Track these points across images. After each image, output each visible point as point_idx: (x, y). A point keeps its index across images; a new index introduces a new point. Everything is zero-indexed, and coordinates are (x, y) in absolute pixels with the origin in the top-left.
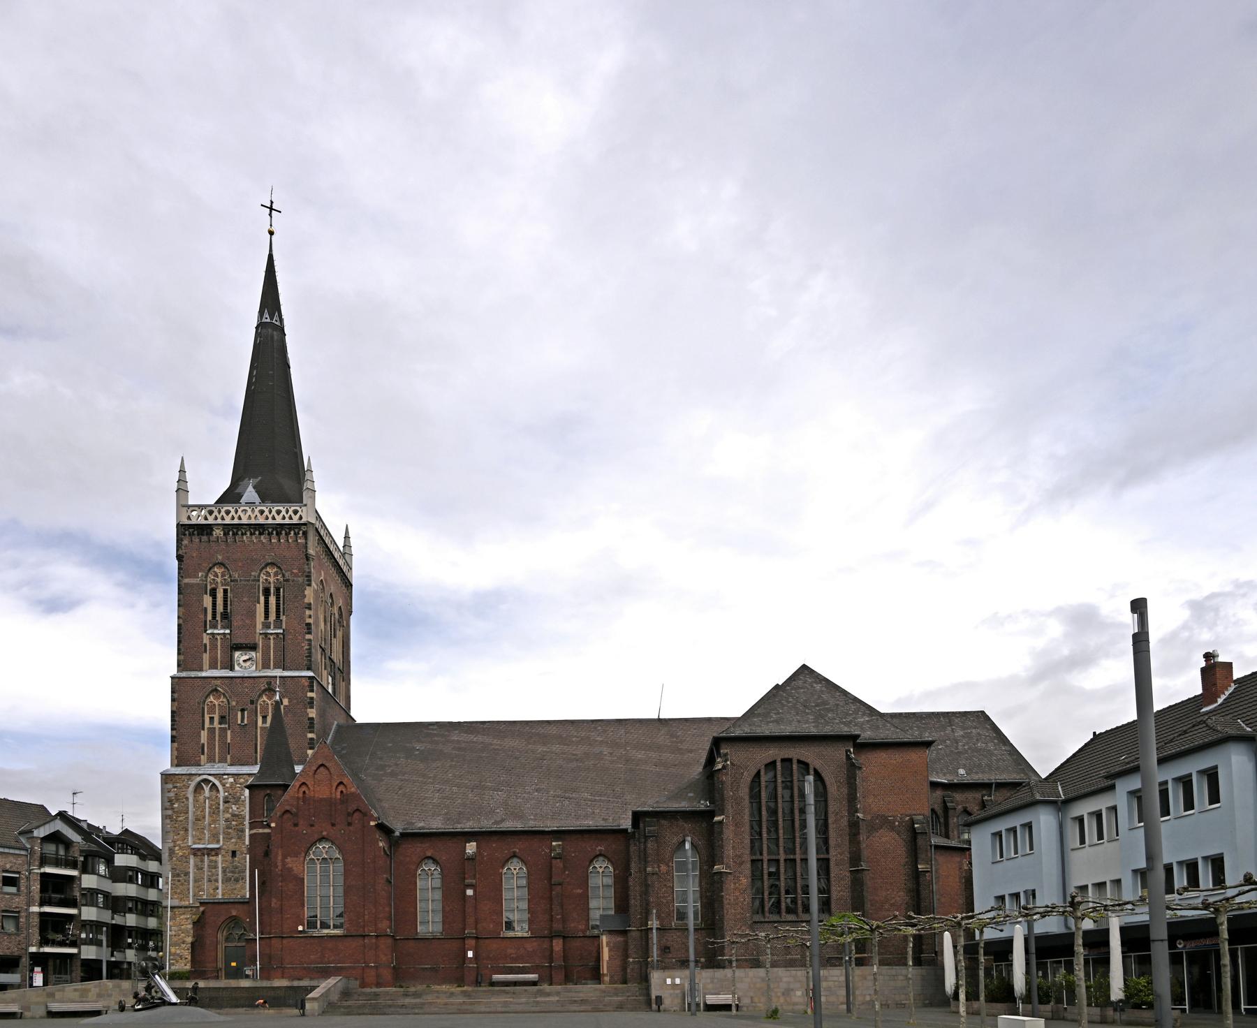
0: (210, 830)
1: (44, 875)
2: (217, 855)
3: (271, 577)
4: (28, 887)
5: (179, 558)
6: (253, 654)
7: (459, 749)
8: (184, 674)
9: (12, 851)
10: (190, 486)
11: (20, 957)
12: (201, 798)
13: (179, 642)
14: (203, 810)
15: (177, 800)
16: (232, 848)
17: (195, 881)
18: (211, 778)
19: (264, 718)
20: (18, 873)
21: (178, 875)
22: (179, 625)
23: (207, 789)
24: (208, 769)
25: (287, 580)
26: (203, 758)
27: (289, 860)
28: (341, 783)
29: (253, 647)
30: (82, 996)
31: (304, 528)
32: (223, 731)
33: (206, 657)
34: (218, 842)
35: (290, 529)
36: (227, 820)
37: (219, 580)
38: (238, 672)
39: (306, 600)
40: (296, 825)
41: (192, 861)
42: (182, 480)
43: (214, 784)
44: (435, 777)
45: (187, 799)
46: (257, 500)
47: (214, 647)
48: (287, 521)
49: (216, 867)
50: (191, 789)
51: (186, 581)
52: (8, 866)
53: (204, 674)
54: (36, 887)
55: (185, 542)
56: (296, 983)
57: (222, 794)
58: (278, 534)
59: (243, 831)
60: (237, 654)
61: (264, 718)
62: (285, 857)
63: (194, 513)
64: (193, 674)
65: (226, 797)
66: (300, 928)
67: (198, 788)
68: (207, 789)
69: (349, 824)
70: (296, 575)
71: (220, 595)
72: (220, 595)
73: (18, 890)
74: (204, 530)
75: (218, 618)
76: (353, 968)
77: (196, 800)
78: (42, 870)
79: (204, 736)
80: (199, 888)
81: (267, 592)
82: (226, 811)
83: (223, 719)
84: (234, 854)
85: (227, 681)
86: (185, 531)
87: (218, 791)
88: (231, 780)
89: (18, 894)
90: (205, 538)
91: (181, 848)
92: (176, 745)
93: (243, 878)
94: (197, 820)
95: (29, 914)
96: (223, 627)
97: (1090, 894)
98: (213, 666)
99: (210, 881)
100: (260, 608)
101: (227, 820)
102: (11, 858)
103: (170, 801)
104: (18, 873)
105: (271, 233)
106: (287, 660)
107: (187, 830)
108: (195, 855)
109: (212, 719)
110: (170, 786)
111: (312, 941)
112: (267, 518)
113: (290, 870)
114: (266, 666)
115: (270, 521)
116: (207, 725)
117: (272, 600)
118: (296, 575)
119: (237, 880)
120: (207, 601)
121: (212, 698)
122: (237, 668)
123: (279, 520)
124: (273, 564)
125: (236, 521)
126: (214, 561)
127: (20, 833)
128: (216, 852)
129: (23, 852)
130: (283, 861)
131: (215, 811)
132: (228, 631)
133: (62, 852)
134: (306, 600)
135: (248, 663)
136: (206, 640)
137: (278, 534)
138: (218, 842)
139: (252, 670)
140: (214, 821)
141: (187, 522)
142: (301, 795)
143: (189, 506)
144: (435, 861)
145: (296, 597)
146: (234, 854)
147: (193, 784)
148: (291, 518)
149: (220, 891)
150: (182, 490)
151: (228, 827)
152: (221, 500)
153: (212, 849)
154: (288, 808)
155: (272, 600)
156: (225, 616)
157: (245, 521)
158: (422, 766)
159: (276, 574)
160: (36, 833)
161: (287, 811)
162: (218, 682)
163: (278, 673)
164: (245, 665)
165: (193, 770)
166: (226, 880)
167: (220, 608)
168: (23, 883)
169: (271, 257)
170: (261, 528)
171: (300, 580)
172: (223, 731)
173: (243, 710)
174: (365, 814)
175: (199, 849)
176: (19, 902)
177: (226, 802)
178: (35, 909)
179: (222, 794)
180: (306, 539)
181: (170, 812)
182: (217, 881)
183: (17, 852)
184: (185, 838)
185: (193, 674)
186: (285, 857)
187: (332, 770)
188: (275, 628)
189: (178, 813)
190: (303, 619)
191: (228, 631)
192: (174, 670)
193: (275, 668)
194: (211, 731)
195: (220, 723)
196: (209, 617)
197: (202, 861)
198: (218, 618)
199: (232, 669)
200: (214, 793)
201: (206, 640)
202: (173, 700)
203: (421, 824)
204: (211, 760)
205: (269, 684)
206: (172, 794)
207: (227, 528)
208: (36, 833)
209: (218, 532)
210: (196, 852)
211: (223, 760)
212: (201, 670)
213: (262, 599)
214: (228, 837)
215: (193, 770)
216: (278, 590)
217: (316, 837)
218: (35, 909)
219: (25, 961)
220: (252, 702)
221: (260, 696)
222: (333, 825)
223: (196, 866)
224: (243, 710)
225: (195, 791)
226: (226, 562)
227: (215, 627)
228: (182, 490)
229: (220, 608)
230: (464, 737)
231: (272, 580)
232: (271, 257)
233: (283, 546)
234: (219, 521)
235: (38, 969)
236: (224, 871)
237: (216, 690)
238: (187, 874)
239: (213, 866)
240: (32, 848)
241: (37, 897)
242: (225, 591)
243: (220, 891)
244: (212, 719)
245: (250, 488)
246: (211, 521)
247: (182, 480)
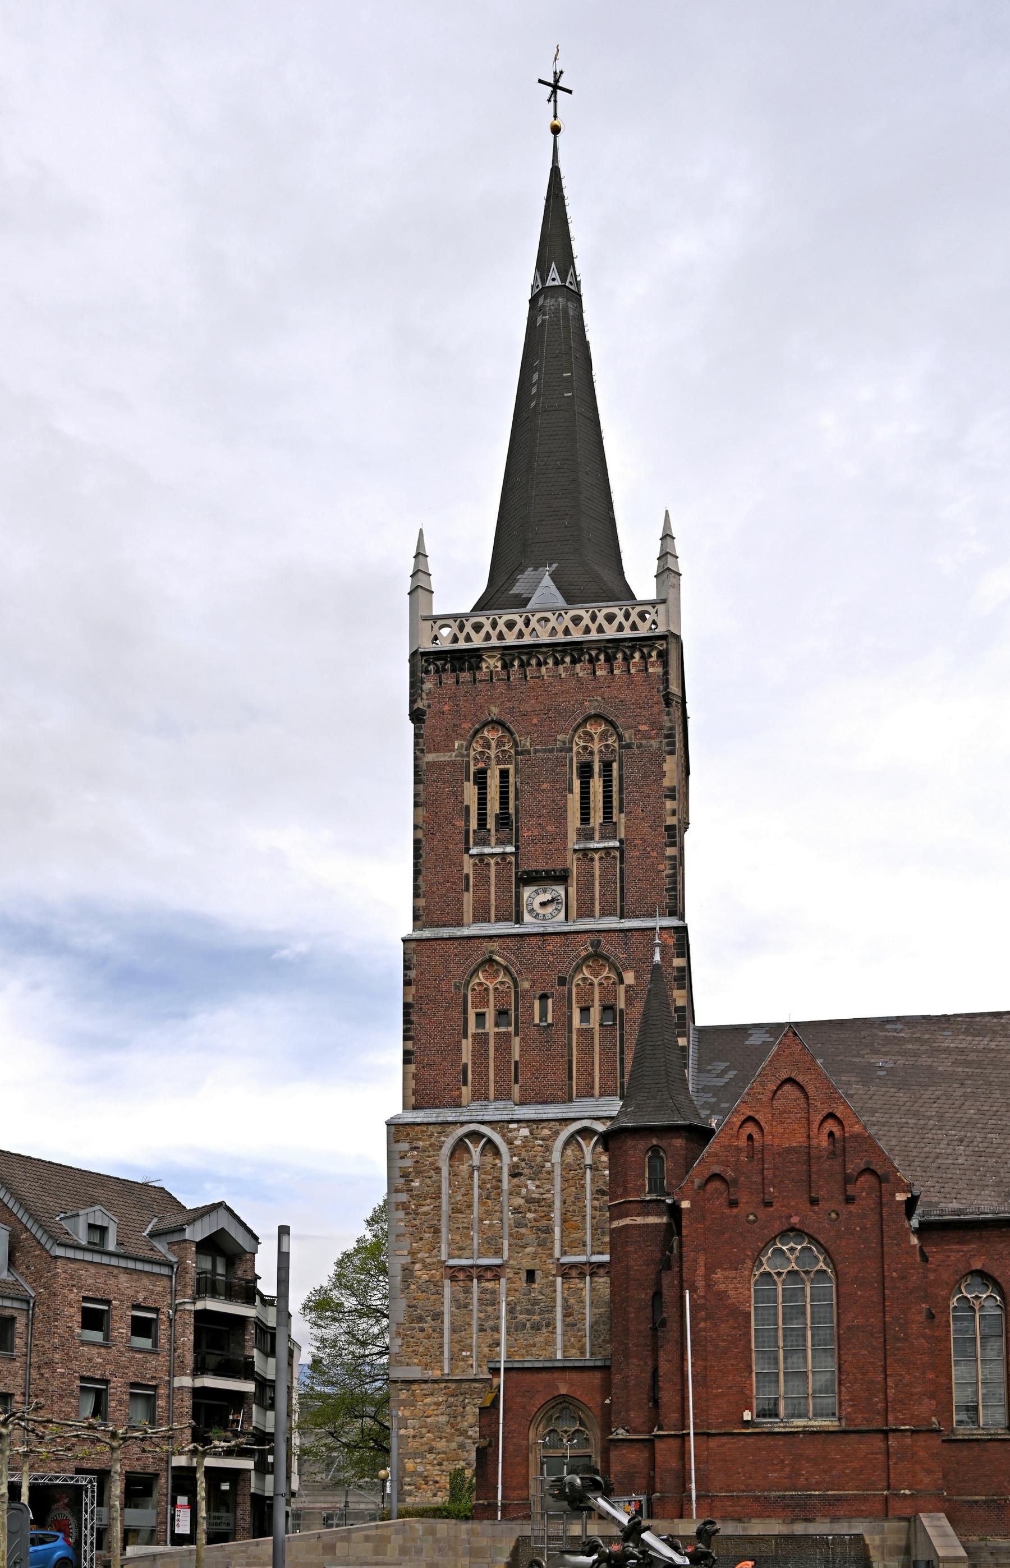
0: (481, 1231)
1: (201, 1316)
2: (497, 1278)
3: (597, 742)
4: (172, 1339)
5: (416, 716)
6: (560, 890)
7: (968, 1063)
8: (427, 933)
9: (148, 1268)
10: (435, 583)
11: (156, 1476)
12: (465, 1167)
13: (417, 873)
14: (468, 1193)
15: (418, 1173)
16: (527, 1264)
17: (454, 1331)
18: (484, 1129)
19: (585, 1010)
20: (156, 1310)
21: (421, 1319)
22: (417, 842)
23: (475, 1150)
24: (473, 1113)
25: (628, 746)
26: (466, 1091)
27: (719, 1275)
28: (831, 1116)
29: (562, 878)
30: (376, 1552)
31: (661, 645)
32: (504, 1039)
33: (468, 898)
34: (498, 1253)
35: (633, 649)
36: (516, 1211)
37: (493, 753)
38: (530, 924)
39: (666, 782)
40: (733, 1204)
41: (447, 1291)
42: (420, 572)
43: (490, 1141)
44: (941, 1117)
45: (438, 1170)
46: (561, 602)
47: (483, 879)
48: (627, 633)
49: (494, 1303)
50: (446, 1150)
51: (430, 757)
52: (141, 1297)
53: (465, 932)
54: (188, 1339)
55: (428, 686)
56: (799, 1528)
57: (506, 1160)
58: (609, 660)
59: (549, 1231)
60: (527, 892)
61: (585, 1010)
62: (710, 1269)
63: (445, 632)
64: (445, 932)
65: (514, 1166)
66: (747, 1416)
67: (460, 1147)
68: (475, 1150)
69: (849, 1200)
70: (646, 736)
71: (493, 782)
72: (493, 782)
73: (155, 1344)
74: (463, 660)
75: (491, 824)
76: (865, 1499)
77: (453, 1174)
78: (200, 1305)
79: (467, 1045)
80: (461, 1345)
81: (585, 771)
82: (515, 1192)
83: (502, 1014)
84: (531, 1275)
85: (511, 943)
86: (424, 663)
87: (497, 1153)
88: (525, 1132)
89: (154, 1352)
90: (466, 676)
91: (425, 1267)
92: (412, 1068)
93: (550, 1324)
94: (456, 1210)
95: (174, 1392)
96: (500, 842)
97: (253, 1484)
98: (481, 916)
99: (482, 1329)
100: (574, 800)
101: (516, 1211)
102: (146, 1281)
103: (405, 1175)
104: (156, 1310)
105: (556, 130)
106: (630, 897)
107: (437, 1231)
108: (453, 1279)
109: (480, 1016)
110: (404, 1146)
111: (770, 1441)
112: (587, 630)
113: (722, 1296)
114: (585, 911)
115: (594, 636)
116: (472, 1029)
117: (597, 784)
118: (646, 736)
119: (536, 1328)
120: (470, 792)
121: (481, 977)
122: (527, 918)
123: (611, 632)
124: (598, 717)
125: (527, 640)
126: (485, 717)
127: (153, 1235)
128: (495, 1272)
129: (165, 1271)
130: (707, 1277)
131: (492, 1192)
132: (510, 849)
133: (221, 1270)
134: (666, 782)
135: (550, 909)
136: (468, 868)
137: (609, 660)
138: (498, 1253)
139: (556, 921)
140: (489, 1214)
141: (431, 647)
142: (743, 1142)
143: (435, 619)
144: (985, 1277)
145: (645, 777)
146: (531, 1275)
147: (449, 1142)
148: (634, 627)
149: (503, 1349)
150: (420, 588)
151: (519, 1224)
152: (481, 606)
153: (488, 1268)
154: (717, 1169)
155: (597, 784)
156: (503, 820)
157: (545, 638)
158: (902, 1096)
159: (604, 736)
160: (188, 1235)
161: (715, 1176)
162: (495, 946)
163: (612, 923)
164: (542, 911)
165: (449, 1115)
166: (516, 1327)
167: (493, 807)
168: (163, 1328)
169: (555, 173)
170: (575, 650)
171: (654, 743)
172: (504, 1039)
173: (544, 997)
174: (881, 1179)
175: (462, 1268)
176: (155, 1367)
177: (514, 1175)
178: (186, 1381)
179: (506, 1160)
180: (665, 665)
181: (403, 1197)
182: (496, 1329)
183: (156, 1269)
184: (434, 1247)
185: (445, 932)
186: (710, 1269)
187: (811, 1090)
188: (603, 837)
189: (419, 1197)
190: (661, 817)
191: (510, 849)
192: (406, 927)
193: (603, 914)
194: (481, 1040)
195: (497, 1025)
196: (474, 825)
197: (467, 1291)
198: (491, 824)
199: (519, 920)
200: (489, 1158)
201: (468, 867)
202: (407, 983)
203: (955, 1205)
204: (480, 1095)
205: (596, 944)
206: (408, 1163)
207: (508, 654)
208: (188, 1235)
209: (492, 663)
210: (454, 1273)
211: (504, 1095)
212: (460, 924)
213: (577, 784)
214: (518, 1244)
215: (449, 1115)
216: (607, 766)
217: (778, 1226)
218: (186, 1381)
219: (164, 1484)
220: (562, 981)
221: (578, 968)
222: (814, 1202)
223: (455, 1300)
224: (544, 997)
225: (452, 1156)
226: (506, 718)
227: (484, 842)
228: (420, 588)
229: (493, 807)
230: (965, 1042)
231: (596, 746)
232: (555, 173)
233: (619, 683)
234: (494, 642)
235: (183, 1500)
236: (511, 1311)
237: (491, 961)
238: (438, 1316)
239: (490, 1300)
240: (181, 1262)
241: (189, 1359)
242: (504, 774)
243: (503, 1349)
244: (480, 1016)
245: (547, 580)
246: (478, 641)
247: (420, 572)
